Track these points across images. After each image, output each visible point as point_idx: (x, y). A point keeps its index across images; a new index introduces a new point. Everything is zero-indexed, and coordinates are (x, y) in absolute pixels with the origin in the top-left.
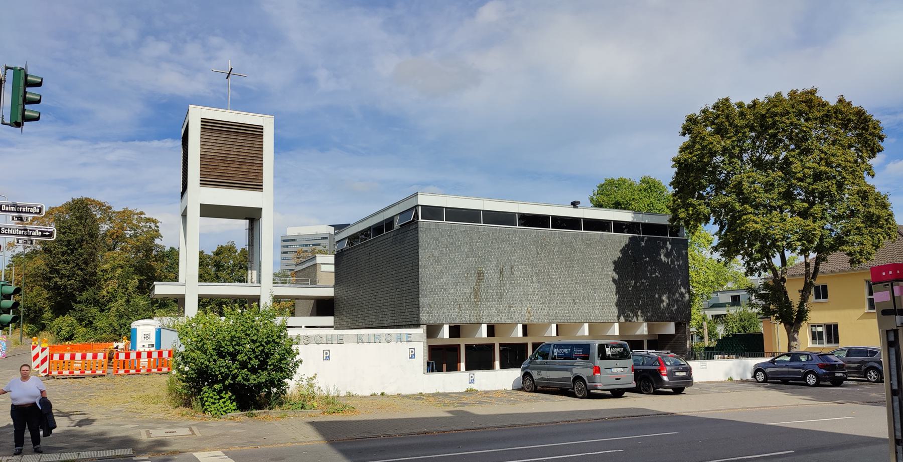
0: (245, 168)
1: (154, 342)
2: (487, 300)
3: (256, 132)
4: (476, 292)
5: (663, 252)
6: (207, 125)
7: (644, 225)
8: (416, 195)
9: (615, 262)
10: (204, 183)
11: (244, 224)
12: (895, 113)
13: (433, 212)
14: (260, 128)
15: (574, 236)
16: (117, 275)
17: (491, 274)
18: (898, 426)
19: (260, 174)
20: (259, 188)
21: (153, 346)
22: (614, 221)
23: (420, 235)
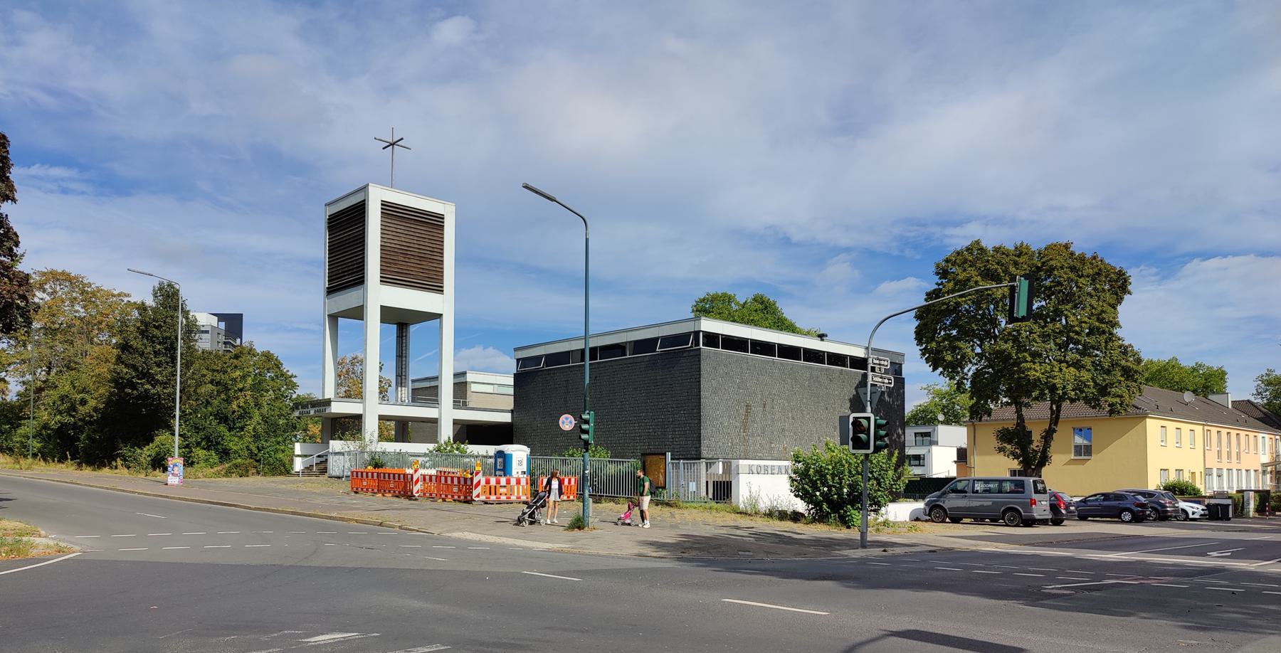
2: (753, 435)
3: (434, 223)
4: (745, 426)
6: (389, 209)
7: (806, 350)
10: (384, 281)
11: (413, 329)
12: (924, 225)
13: (712, 339)
14: (441, 217)
15: (822, 370)
16: (248, 386)
17: (757, 409)
18: (898, 551)
19: (440, 273)
20: (440, 290)
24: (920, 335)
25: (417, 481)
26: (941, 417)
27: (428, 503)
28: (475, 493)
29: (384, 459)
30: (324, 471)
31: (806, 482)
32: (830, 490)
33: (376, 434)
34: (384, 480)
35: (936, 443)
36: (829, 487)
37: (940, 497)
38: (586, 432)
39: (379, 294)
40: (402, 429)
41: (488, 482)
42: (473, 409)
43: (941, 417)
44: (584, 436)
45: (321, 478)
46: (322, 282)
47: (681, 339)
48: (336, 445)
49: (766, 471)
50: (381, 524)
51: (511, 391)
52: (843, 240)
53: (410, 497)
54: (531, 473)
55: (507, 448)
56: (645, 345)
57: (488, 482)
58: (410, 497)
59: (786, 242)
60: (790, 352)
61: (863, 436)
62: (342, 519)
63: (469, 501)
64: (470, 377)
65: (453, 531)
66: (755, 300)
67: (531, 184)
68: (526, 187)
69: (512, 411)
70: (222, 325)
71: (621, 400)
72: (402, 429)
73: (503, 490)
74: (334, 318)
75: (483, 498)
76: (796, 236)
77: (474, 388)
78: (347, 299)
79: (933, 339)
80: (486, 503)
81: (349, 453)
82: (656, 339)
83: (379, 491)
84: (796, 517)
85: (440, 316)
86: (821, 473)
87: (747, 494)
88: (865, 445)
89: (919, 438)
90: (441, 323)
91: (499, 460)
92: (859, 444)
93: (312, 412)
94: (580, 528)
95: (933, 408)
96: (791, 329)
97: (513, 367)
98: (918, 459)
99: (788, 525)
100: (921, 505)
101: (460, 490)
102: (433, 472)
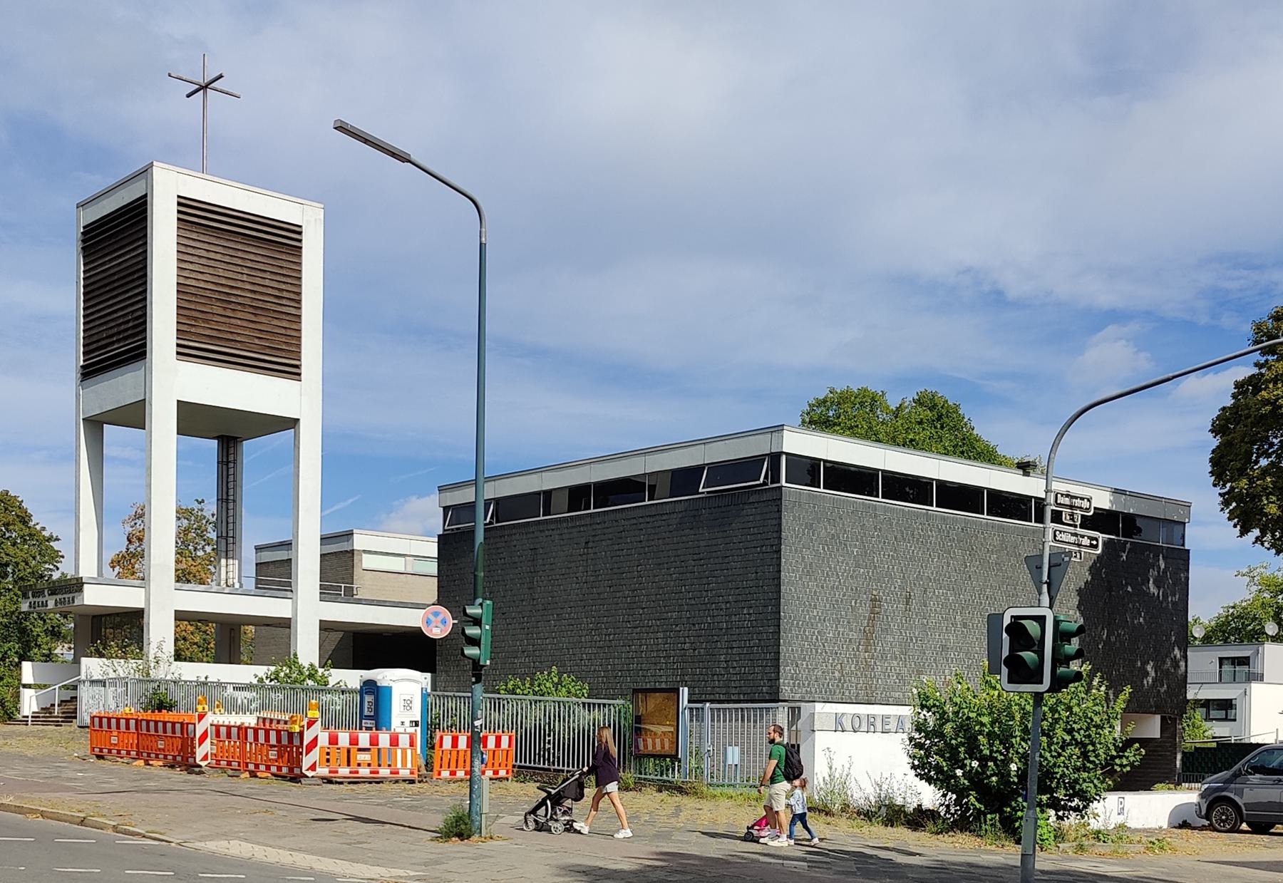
2: (884, 657)
3: (284, 240)
4: (868, 639)
5: (1153, 573)
7: (942, 485)
8: (780, 428)
9: (1080, 592)
10: (184, 353)
11: (251, 449)
13: (808, 470)
14: (296, 230)
17: (892, 607)
20: (293, 372)
21: (417, 724)
22: (883, 471)
23: (784, 513)
24: (1222, 466)
25: (204, 736)
26: (1271, 628)
27: (220, 781)
28: (307, 761)
29: (178, 695)
30: (71, 716)
31: (939, 751)
32: (983, 765)
33: (170, 648)
34: (159, 736)
35: (1260, 678)
36: (983, 761)
37: (1228, 781)
38: (474, 642)
39: (174, 378)
40: (222, 638)
41: (333, 740)
42: (359, 602)
43: (1271, 628)
44: (471, 651)
45: (65, 728)
46: (74, 357)
47: (748, 467)
48: (92, 666)
49: (871, 725)
50: (82, 822)
51: (433, 568)
52: (1105, 296)
53: (192, 768)
54: (431, 727)
55: (384, 676)
56: (684, 479)
57: (333, 740)
58: (192, 768)
59: (997, 299)
60: (960, 497)
61: (1028, 655)
62: (19, 810)
63: (296, 778)
64: (360, 541)
65: (211, 837)
66: (919, 402)
67: (352, 122)
68: (342, 128)
71: (624, 590)
72: (222, 638)
74: (95, 425)
75: (323, 771)
76: (1016, 287)
77: (368, 562)
78: (116, 389)
79: (1242, 472)
80: (330, 782)
81: (114, 682)
82: (698, 470)
83: (139, 756)
84: (919, 819)
85: (293, 423)
86: (967, 730)
88: (1034, 675)
89: (1227, 668)
90: (297, 437)
91: (368, 698)
92: (1021, 672)
93: (51, 604)
94: (461, 836)
95: (1260, 613)
96: (986, 456)
97: (437, 524)
98: (1225, 708)
99: (901, 835)
100: (1189, 796)
101: (280, 756)
102: (250, 720)
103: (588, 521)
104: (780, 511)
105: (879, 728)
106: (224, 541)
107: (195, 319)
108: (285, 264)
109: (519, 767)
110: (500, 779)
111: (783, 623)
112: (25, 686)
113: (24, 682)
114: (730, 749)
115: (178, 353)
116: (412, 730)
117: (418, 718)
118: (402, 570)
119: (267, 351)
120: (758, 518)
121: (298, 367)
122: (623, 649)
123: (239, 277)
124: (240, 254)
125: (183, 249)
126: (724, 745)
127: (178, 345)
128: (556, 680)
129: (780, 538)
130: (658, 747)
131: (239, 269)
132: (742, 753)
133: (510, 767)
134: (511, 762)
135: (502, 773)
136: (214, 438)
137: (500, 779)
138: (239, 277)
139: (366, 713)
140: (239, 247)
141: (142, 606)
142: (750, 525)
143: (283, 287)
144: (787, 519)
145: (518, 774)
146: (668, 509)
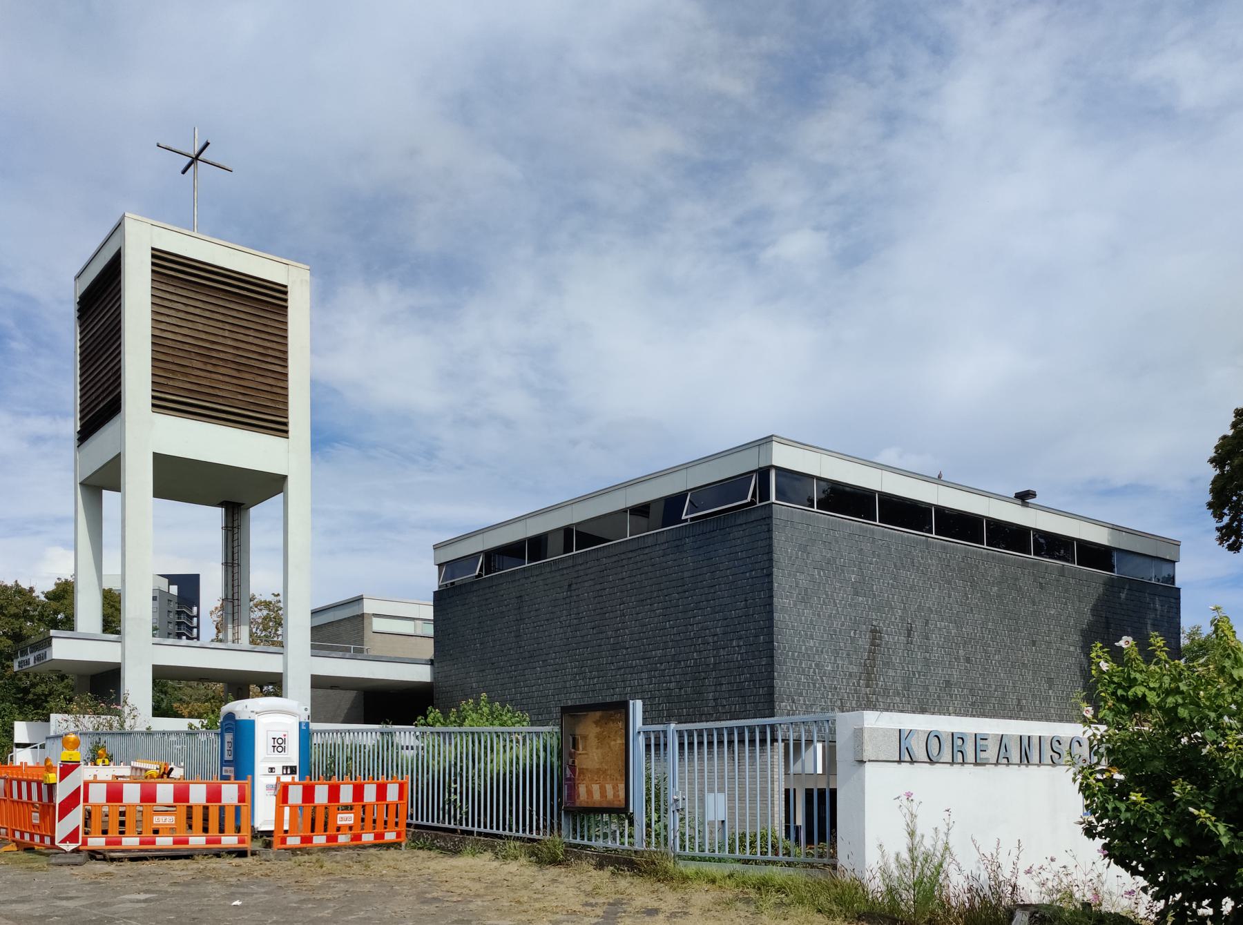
0: (251, 380)
1: (295, 762)
7: (941, 510)
10: (161, 404)
13: (793, 481)
14: (282, 290)
15: (1023, 565)
20: (279, 428)
21: (293, 770)
22: (882, 494)
23: (776, 534)
39: (148, 431)
46: (72, 426)
47: (733, 486)
49: (959, 752)
51: (430, 630)
69: (432, 662)
70: (174, 590)
73: (346, 819)
77: (378, 625)
87: (898, 845)
91: (229, 737)
103: (570, 562)
104: (770, 531)
105: (970, 757)
106: (230, 605)
107: (174, 372)
108: (269, 323)
109: (417, 826)
110: (389, 846)
111: (778, 654)
112: (19, 746)
113: (16, 740)
114: (710, 798)
115: (153, 405)
116: (287, 779)
117: (295, 763)
118: (412, 632)
119: (252, 407)
120: (746, 540)
121: (286, 424)
122: (608, 693)
123: (220, 332)
124: (221, 310)
125: (158, 301)
126: (701, 791)
127: (153, 397)
128: (486, 710)
129: (771, 560)
130: (597, 796)
131: (220, 325)
132: (731, 799)
133: (403, 828)
134: (403, 821)
135: (390, 836)
136: (220, 505)
137: (389, 846)
138: (220, 332)
139: (227, 757)
140: (221, 303)
141: (118, 660)
142: (738, 549)
143: (269, 345)
144: (779, 538)
145: (415, 838)
146: (650, 542)
